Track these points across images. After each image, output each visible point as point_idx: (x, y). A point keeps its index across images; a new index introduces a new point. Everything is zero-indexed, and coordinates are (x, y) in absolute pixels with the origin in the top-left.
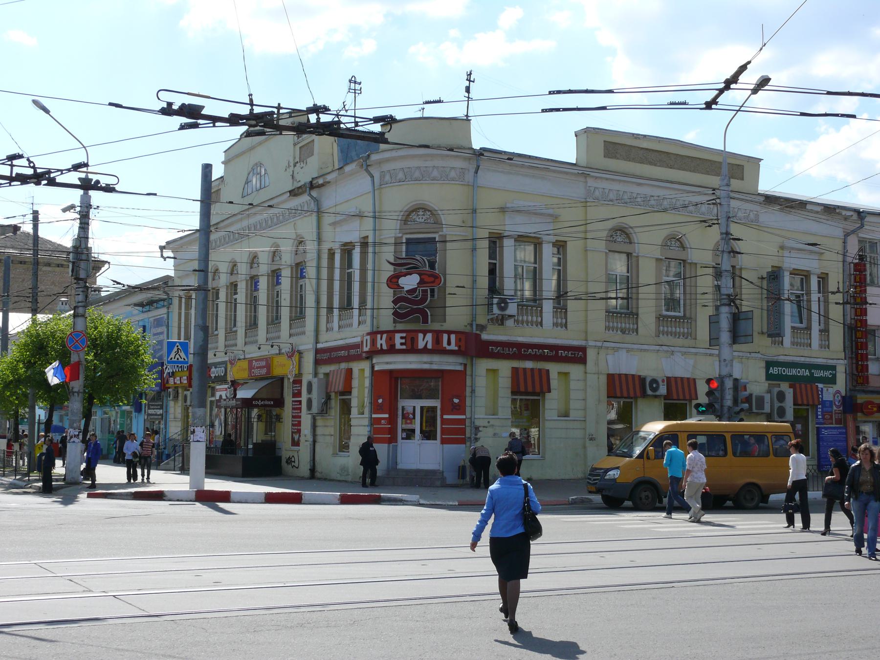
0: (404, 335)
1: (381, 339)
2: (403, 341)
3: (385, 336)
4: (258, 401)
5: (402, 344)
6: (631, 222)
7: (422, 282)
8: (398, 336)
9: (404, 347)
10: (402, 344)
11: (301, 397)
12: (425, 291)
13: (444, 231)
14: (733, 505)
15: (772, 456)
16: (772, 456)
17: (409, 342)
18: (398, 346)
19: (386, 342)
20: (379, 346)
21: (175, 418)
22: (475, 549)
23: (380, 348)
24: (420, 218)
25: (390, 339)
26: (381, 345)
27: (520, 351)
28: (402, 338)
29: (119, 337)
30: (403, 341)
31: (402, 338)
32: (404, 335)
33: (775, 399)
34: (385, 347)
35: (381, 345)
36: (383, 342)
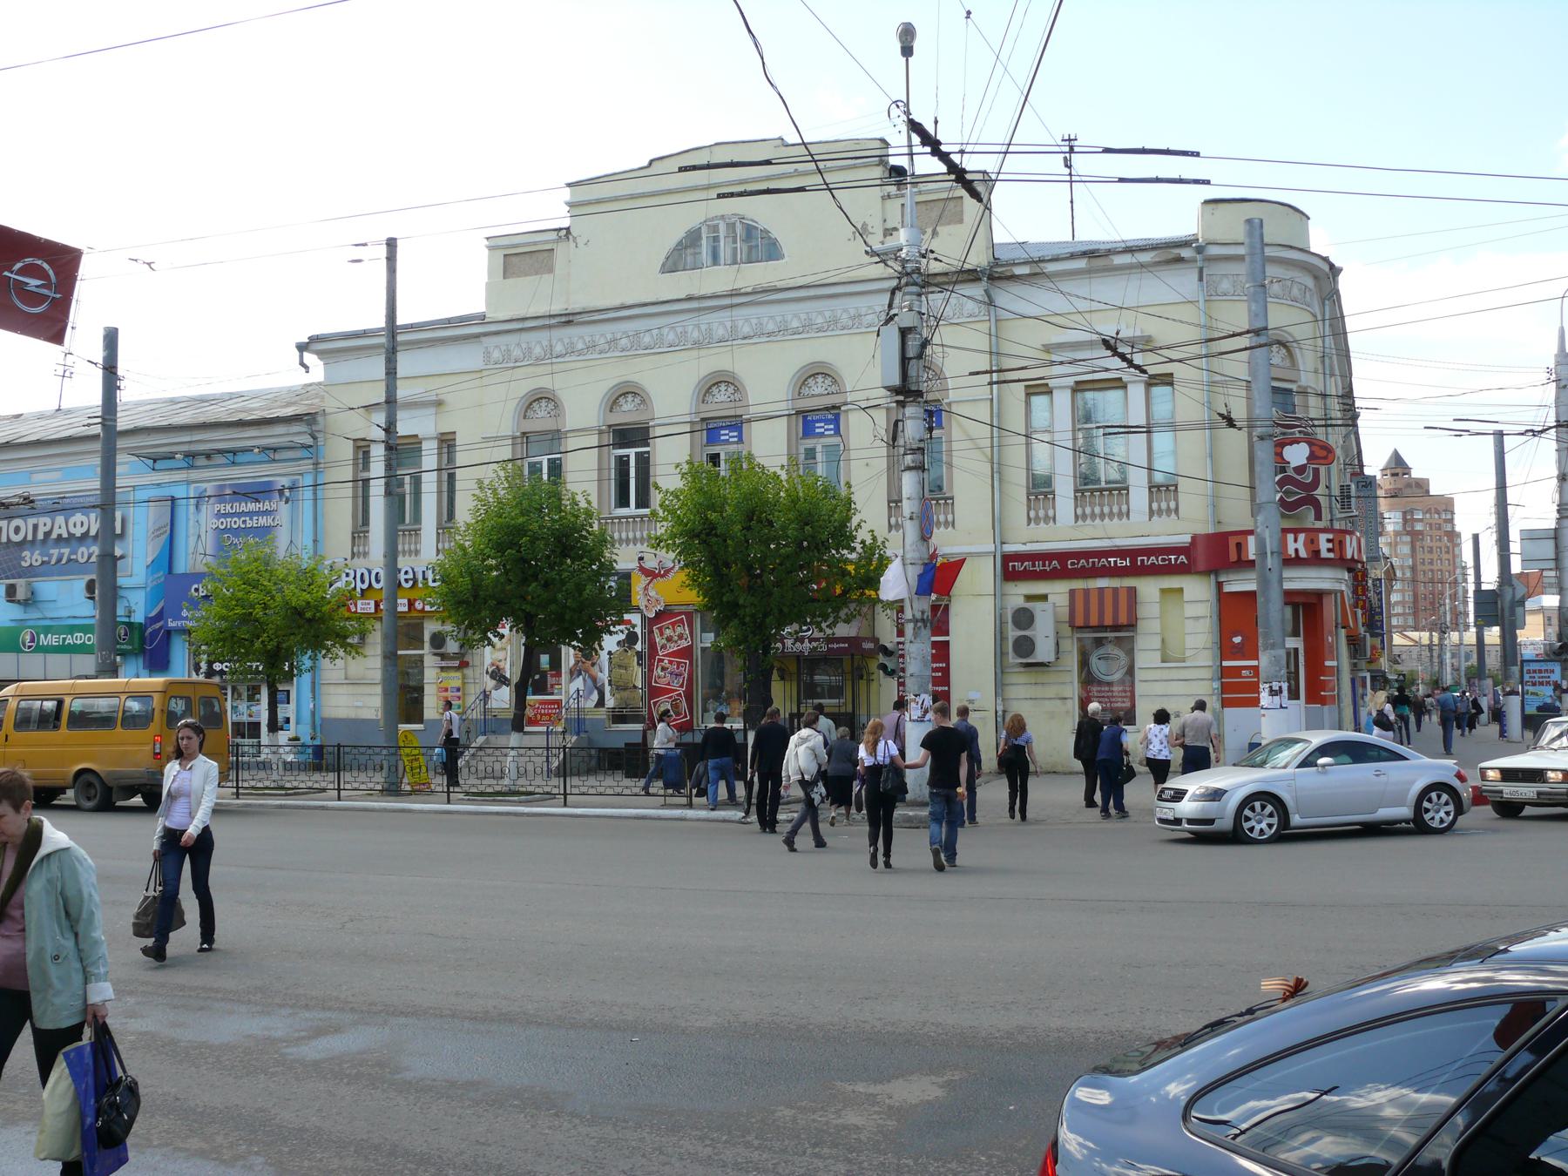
0: (1330, 536)
1: (1296, 541)
2: (1330, 545)
3: (1302, 537)
4: (802, 643)
5: (1329, 550)
6: (545, 383)
7: (1312, 457)
8: (1323, 537)
9: (1331, 555)
10: (1329, 550)
11: (947, 634)
12: (1316, 472)
13: (950, 396)
14: (145, 805)
15: (119, 729)
16: (119, 729)
17: (1337, 548)
18: (1324, 554)
19: (1305, 544)
20: (1291, 552)
21: (346, 679)
22: (795, 846)
23: (1293, 556)
24: (818, 387)
25: (1312, 541)
26: (1296, 550)
27: (1063, 564)
28: (1329, 541)
29: (446, 569)
30: (1330, 545)
31: (1329, 541)
32: (1330, 536)
33: (1010, 625)
34: (1303, 554)
35: (1296, 550)
36: (1300, 545)
